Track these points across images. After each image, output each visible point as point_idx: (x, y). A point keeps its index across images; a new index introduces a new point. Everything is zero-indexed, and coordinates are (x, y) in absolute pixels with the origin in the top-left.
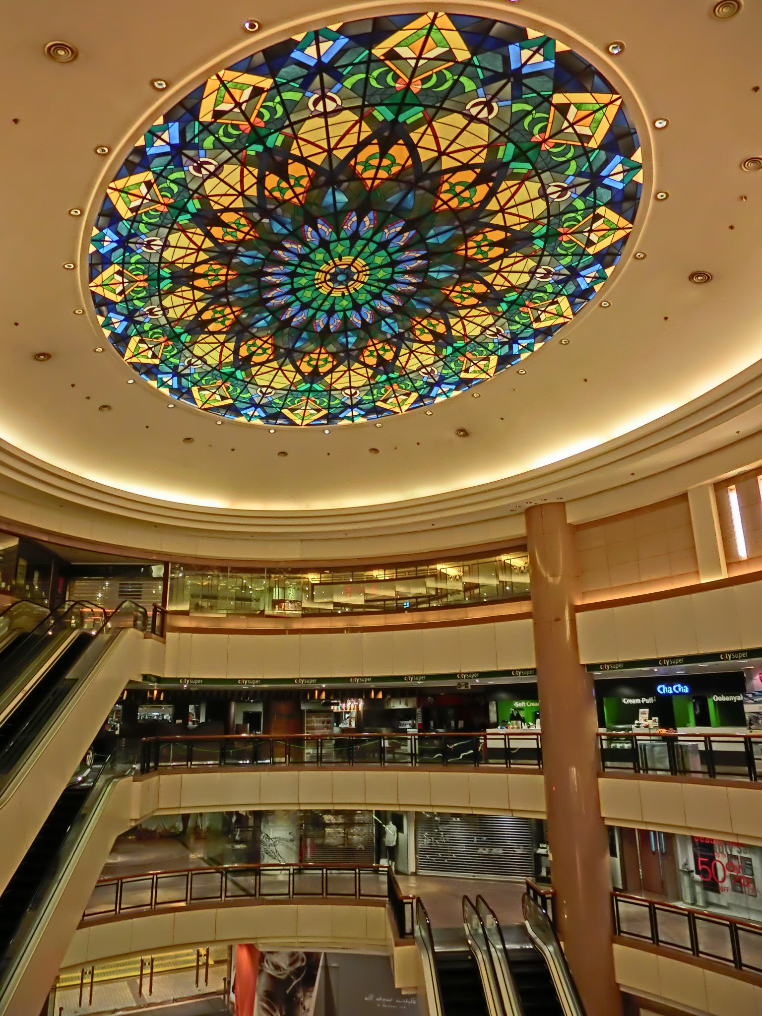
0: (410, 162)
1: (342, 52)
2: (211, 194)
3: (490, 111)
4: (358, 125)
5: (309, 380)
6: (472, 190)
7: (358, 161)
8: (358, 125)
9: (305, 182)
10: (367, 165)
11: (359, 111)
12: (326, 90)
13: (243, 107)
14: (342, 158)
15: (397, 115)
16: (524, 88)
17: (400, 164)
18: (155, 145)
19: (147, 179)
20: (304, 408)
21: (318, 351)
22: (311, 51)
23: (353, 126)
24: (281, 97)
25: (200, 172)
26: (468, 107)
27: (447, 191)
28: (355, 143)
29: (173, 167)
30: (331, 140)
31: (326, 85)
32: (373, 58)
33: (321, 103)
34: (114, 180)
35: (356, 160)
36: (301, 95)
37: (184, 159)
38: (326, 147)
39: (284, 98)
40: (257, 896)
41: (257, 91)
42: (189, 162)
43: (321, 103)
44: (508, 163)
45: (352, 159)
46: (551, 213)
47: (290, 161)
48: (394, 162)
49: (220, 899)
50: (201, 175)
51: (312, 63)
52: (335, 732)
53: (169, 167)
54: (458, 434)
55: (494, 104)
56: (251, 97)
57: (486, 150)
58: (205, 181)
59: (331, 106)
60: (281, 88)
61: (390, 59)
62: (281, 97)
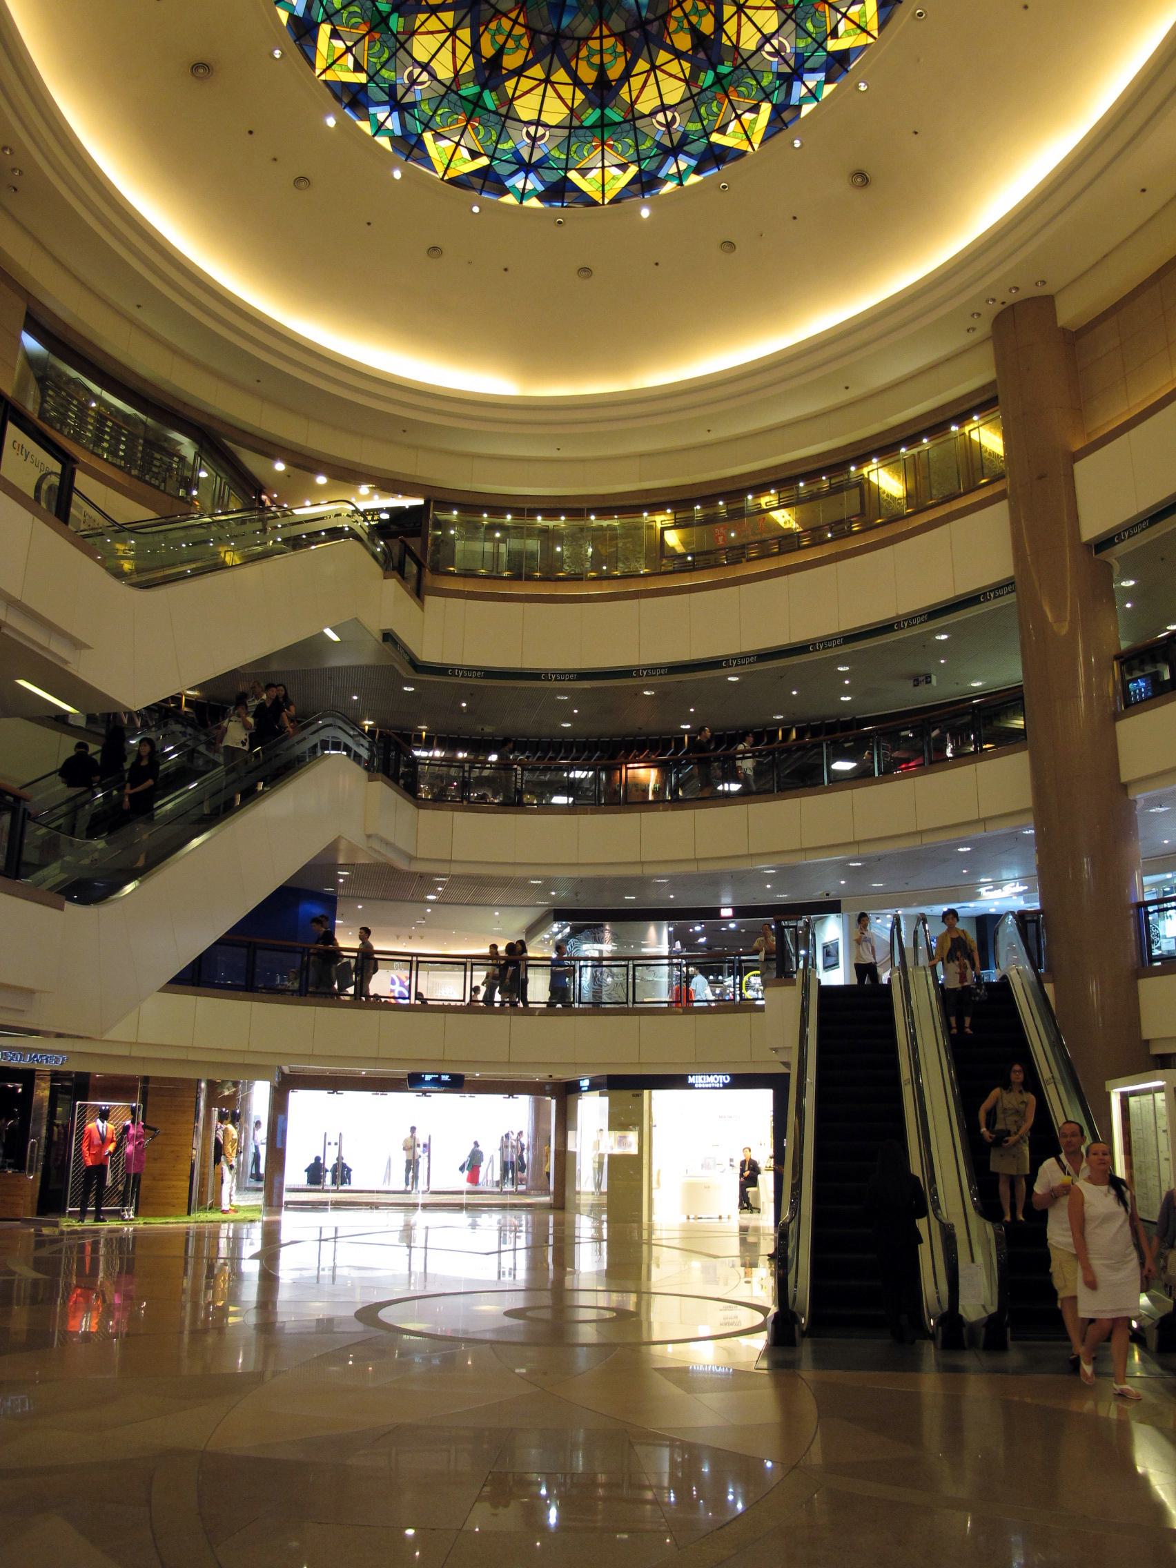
0: (573, 64)
1: (660, 167)
2: (773, 11)
3: (528, 134)
4: (633, 99)
5: (598, 101)
6: (497, 47)
7: (623, 58)
8: (633, 99)
9: (673, 25)
10: (616, 55)
11: (637, 115)
12: (667, 132)
13: (734, 115)
14: (640, 60)
15: (603, 114)
16: (514, 160)
17: (582, 59)
18: (815, 83)
19: (834, 41)
20: (600, 165)
21: (597, 34)
22: (683, 166)
23: (638, 97)
24: (703, 124)
25: (780, 43)
26: (548, 133)
27: (521, 36)
28: (631, 79)
29: (805, 54)
30: (654, 81)
31: (668, 136)
32: (637, 163)
33: (669, 119)
34: (867, 45)
35: (626, 58)
36: (688, 129)
37: (792, 62)
38: (657, 71)
39: (699, 124)
40: (631, 966)
41: (722, 130)
42: (787, 58)
43: (669, 119)
44: (483, 90)
45: (630, 58)
46: (402, 50)
47: (690, 53)
48: (588, 59)
49: (626, 1006)
50: (781, 39)
51: (681, 156)
52: (666, 929)
53: (809, 54)
54: (743, 1163)
55: (528, 141)
56: (727, 125)
57: (510, 96)
58: (777, 31)
59: (660, 117)
60: (703, 134)
61: (625, 164)
62: (703, 124)
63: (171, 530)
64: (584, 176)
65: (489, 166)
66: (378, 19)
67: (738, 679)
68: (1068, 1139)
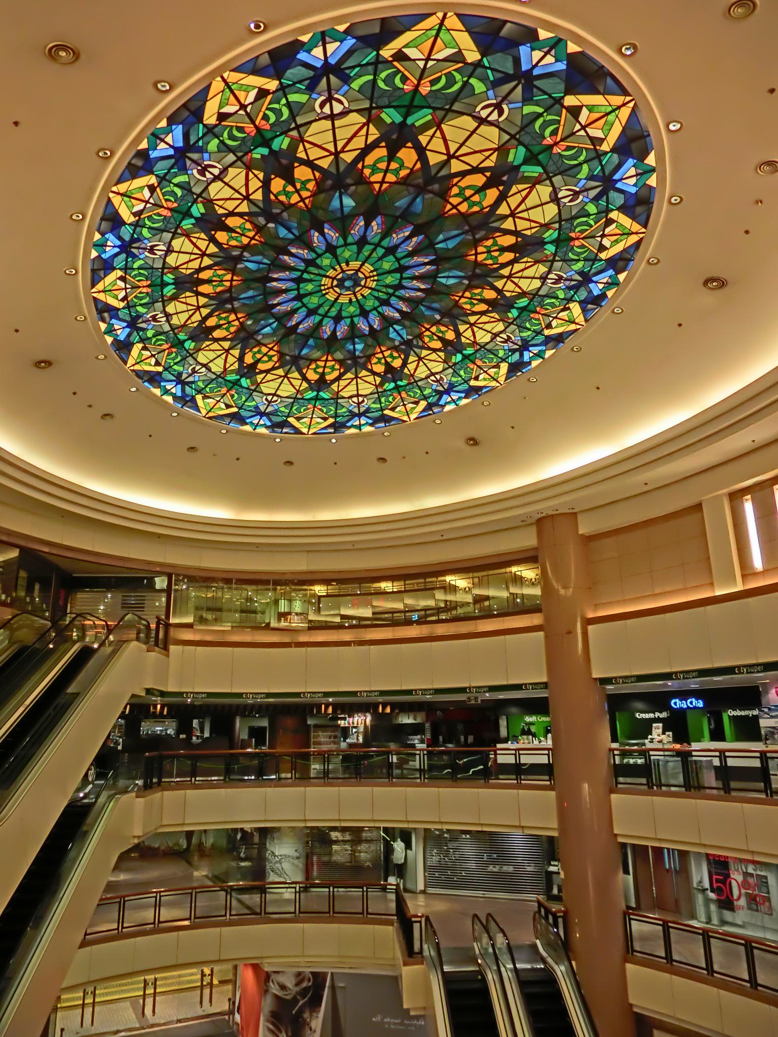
0: (418, 165)
1: (350, 53)
2: (216, 198)
3: (501, 113)
4: (366, 127)
6: (482, 194)
7: (365, 164)
8: (366, 127)
9: (311, 186)
10: (374, 169)
11: (366, 113)
12: (333, 92)
13: (249, 109)
14: (349, 162)
15: (405, 117)
16: (535, 90)
17: (408, 168)
18: (158, 148)
19: (150, 183)
22: (318, 52)
23: (360, 129)
24: (287, 99)
25: (204, 176)
26: (478, 109)
27: (456, 195)
28: (363, 146)
29: (176, 170)
30: (338, 143)
31: (333, 87)
32: (381, 59)
33: (328, 105)
34: (116, 184)
35: (363, 163)
36: (307, 96)
37: (188, 162)
38: (333, 150)
39: (290, 100)
41: (262, 93)
42: (193, 165)
43: (328, 105)
44: (519, 167)
45: (359, 162)
46: (563, 218)
47: (296, 164)
48: (402, 166)
50: (205, 179)
51: (319, 64)
53: (172, 171)
55: (504, 106)
56: (257, 99)
57: (496, 153)
58: (209, 184)
59: (338, 108)
60: (287, 90)
61: (398, 60)
62: (287, 99)
63: (295, 956)
64: (393, 411)
65: (568, 92)
66: (562, 244)
67: (250, 864)
68: (267, 1004)
